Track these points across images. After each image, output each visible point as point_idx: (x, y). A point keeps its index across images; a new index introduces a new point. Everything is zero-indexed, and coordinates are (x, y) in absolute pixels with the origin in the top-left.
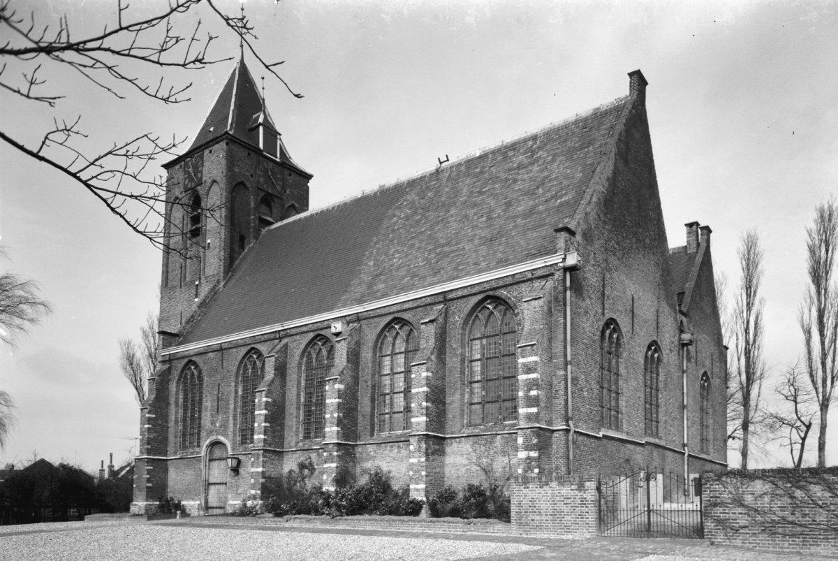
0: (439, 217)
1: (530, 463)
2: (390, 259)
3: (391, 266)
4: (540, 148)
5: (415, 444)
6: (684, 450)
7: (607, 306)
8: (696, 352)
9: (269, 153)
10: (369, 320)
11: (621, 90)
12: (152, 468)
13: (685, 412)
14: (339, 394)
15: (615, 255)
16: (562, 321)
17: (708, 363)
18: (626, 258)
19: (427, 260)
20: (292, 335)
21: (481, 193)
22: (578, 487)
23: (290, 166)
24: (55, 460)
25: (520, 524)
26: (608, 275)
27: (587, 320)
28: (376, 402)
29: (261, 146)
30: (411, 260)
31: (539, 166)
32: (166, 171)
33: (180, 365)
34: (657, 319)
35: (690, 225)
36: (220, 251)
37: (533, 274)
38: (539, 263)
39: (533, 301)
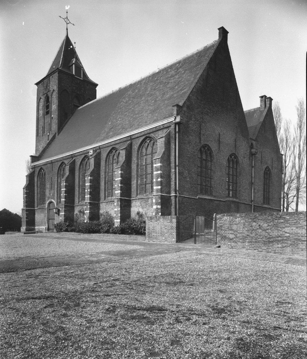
3: (116, 124)
4: (180, 67)
5: (116, 202)
7: (202, 139)
9: (77, 76)
11: (214, 37)
12: (28, 213)
13: (253, 185)
14: (90, 181)
16: (174, 147)
17: (269, 162)
20: (76, 156)
21: (155, 89)
22: (170, 221)
23: (89, 82)
24: (10, 211)
29: (74, 73)
32: (37, 86)
33: (37, 170)
35: (262, 97)
36: (56, 121)
38: (165, 122)
39: (161, 139)
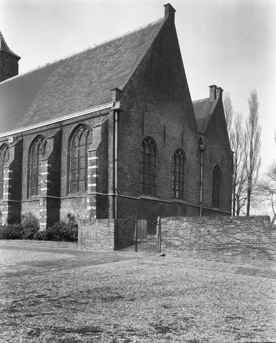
0: (69, 81)
1: (92, 212)
2: (44, 104)
4: (121, 45)
6: (200, 206)
8: (211, 155)
10: (27, 136)
11: (160, 15)
15: (152, 103)
17: (219, 160)
18: (160, 105)
19: (59, 104)
21: (90, 68)
25: (82, 244)
26: (147, 114)
27: (131, 137)
28: (30, 180)
30: (52, 104)
31: (118, 55)
34: (182, 137)
35: (211, 87)
37: (100, 113)
38: (102, 107)
